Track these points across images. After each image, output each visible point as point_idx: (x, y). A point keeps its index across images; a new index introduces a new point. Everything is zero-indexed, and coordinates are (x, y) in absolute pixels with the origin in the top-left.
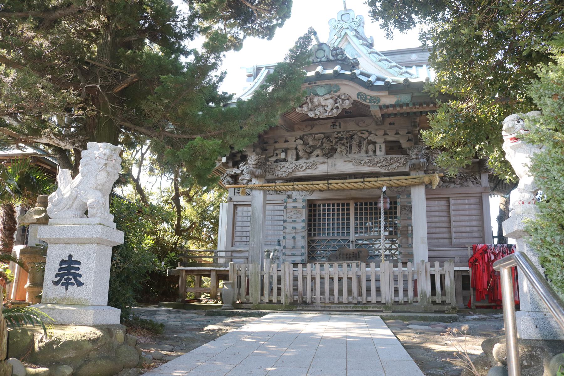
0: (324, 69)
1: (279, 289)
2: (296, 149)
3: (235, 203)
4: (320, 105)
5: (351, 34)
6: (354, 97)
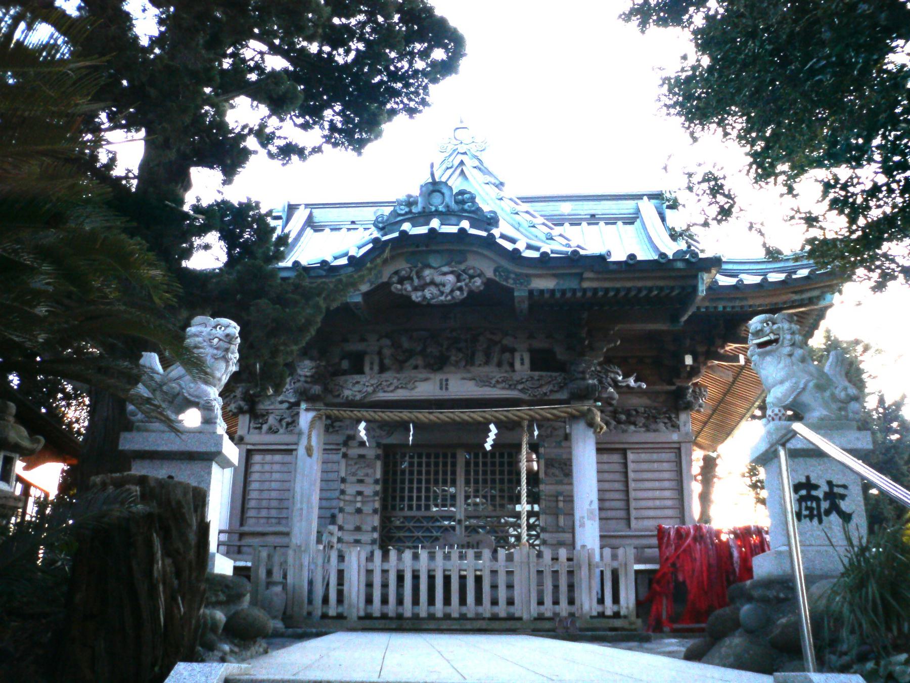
0: (442, 224)
1: (340, 593)
2: (379, 353)
3: (249, 447)
4: (432, 283)
5: (469, 162)
6: (490, 274)
